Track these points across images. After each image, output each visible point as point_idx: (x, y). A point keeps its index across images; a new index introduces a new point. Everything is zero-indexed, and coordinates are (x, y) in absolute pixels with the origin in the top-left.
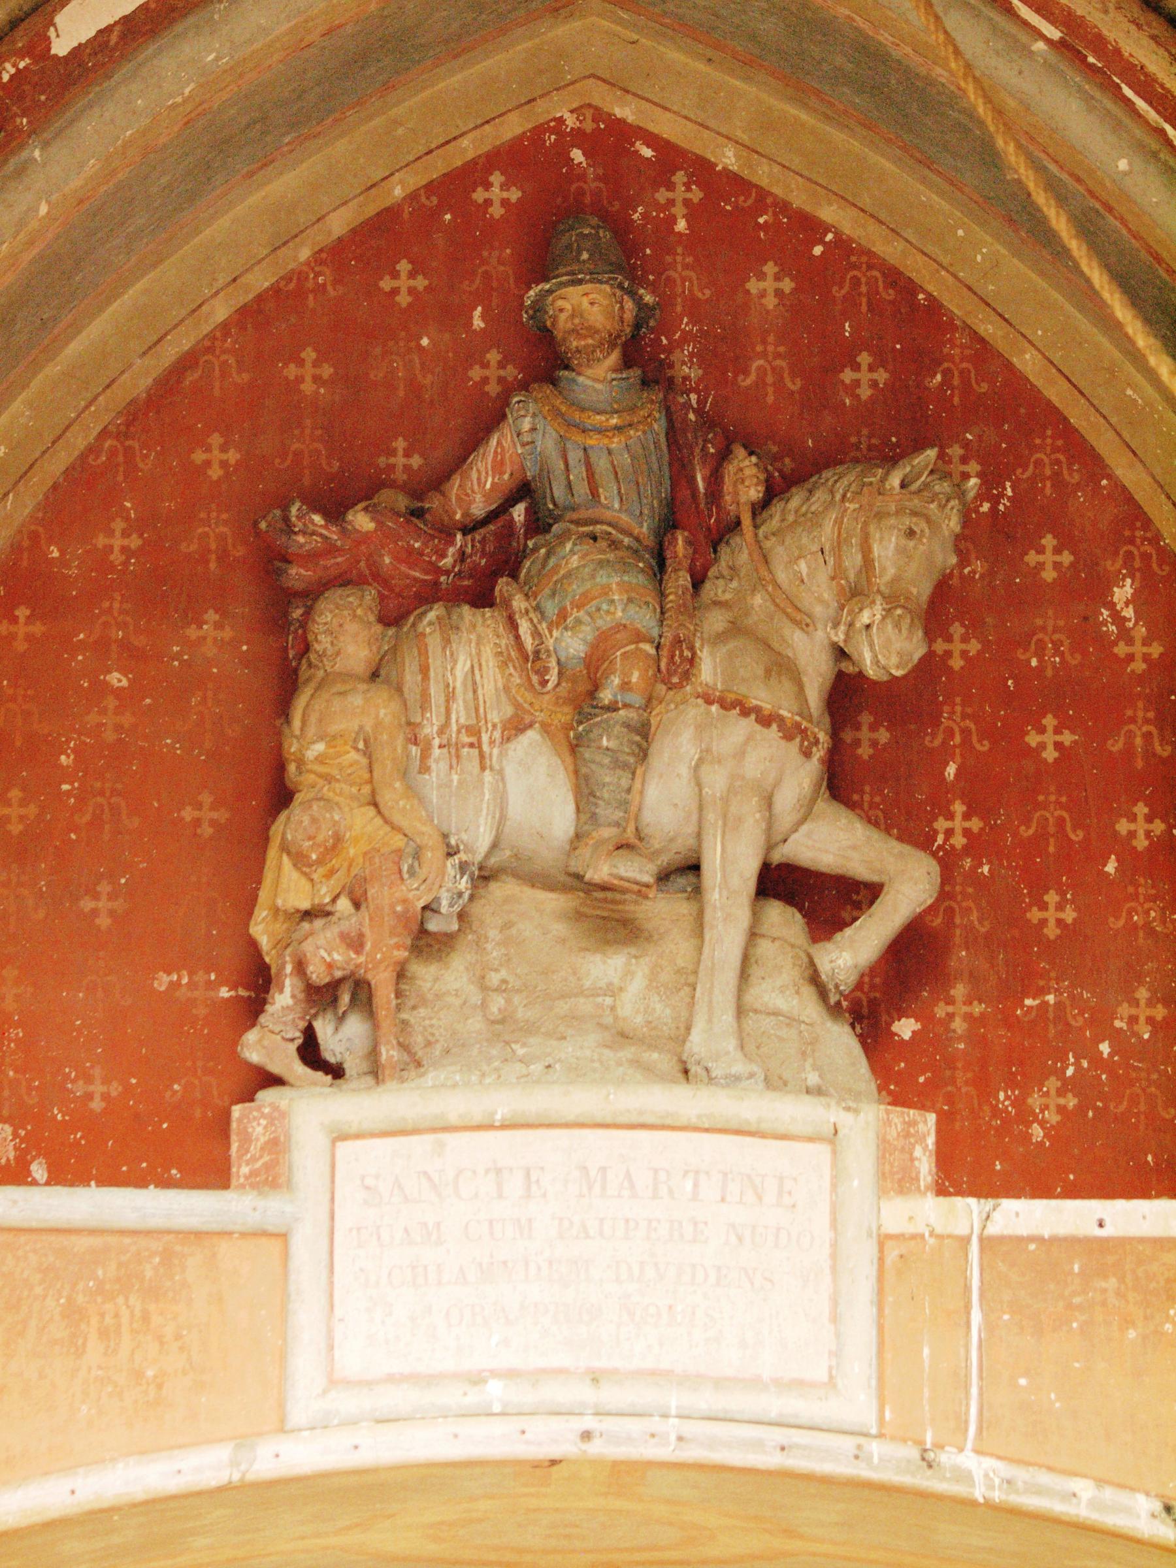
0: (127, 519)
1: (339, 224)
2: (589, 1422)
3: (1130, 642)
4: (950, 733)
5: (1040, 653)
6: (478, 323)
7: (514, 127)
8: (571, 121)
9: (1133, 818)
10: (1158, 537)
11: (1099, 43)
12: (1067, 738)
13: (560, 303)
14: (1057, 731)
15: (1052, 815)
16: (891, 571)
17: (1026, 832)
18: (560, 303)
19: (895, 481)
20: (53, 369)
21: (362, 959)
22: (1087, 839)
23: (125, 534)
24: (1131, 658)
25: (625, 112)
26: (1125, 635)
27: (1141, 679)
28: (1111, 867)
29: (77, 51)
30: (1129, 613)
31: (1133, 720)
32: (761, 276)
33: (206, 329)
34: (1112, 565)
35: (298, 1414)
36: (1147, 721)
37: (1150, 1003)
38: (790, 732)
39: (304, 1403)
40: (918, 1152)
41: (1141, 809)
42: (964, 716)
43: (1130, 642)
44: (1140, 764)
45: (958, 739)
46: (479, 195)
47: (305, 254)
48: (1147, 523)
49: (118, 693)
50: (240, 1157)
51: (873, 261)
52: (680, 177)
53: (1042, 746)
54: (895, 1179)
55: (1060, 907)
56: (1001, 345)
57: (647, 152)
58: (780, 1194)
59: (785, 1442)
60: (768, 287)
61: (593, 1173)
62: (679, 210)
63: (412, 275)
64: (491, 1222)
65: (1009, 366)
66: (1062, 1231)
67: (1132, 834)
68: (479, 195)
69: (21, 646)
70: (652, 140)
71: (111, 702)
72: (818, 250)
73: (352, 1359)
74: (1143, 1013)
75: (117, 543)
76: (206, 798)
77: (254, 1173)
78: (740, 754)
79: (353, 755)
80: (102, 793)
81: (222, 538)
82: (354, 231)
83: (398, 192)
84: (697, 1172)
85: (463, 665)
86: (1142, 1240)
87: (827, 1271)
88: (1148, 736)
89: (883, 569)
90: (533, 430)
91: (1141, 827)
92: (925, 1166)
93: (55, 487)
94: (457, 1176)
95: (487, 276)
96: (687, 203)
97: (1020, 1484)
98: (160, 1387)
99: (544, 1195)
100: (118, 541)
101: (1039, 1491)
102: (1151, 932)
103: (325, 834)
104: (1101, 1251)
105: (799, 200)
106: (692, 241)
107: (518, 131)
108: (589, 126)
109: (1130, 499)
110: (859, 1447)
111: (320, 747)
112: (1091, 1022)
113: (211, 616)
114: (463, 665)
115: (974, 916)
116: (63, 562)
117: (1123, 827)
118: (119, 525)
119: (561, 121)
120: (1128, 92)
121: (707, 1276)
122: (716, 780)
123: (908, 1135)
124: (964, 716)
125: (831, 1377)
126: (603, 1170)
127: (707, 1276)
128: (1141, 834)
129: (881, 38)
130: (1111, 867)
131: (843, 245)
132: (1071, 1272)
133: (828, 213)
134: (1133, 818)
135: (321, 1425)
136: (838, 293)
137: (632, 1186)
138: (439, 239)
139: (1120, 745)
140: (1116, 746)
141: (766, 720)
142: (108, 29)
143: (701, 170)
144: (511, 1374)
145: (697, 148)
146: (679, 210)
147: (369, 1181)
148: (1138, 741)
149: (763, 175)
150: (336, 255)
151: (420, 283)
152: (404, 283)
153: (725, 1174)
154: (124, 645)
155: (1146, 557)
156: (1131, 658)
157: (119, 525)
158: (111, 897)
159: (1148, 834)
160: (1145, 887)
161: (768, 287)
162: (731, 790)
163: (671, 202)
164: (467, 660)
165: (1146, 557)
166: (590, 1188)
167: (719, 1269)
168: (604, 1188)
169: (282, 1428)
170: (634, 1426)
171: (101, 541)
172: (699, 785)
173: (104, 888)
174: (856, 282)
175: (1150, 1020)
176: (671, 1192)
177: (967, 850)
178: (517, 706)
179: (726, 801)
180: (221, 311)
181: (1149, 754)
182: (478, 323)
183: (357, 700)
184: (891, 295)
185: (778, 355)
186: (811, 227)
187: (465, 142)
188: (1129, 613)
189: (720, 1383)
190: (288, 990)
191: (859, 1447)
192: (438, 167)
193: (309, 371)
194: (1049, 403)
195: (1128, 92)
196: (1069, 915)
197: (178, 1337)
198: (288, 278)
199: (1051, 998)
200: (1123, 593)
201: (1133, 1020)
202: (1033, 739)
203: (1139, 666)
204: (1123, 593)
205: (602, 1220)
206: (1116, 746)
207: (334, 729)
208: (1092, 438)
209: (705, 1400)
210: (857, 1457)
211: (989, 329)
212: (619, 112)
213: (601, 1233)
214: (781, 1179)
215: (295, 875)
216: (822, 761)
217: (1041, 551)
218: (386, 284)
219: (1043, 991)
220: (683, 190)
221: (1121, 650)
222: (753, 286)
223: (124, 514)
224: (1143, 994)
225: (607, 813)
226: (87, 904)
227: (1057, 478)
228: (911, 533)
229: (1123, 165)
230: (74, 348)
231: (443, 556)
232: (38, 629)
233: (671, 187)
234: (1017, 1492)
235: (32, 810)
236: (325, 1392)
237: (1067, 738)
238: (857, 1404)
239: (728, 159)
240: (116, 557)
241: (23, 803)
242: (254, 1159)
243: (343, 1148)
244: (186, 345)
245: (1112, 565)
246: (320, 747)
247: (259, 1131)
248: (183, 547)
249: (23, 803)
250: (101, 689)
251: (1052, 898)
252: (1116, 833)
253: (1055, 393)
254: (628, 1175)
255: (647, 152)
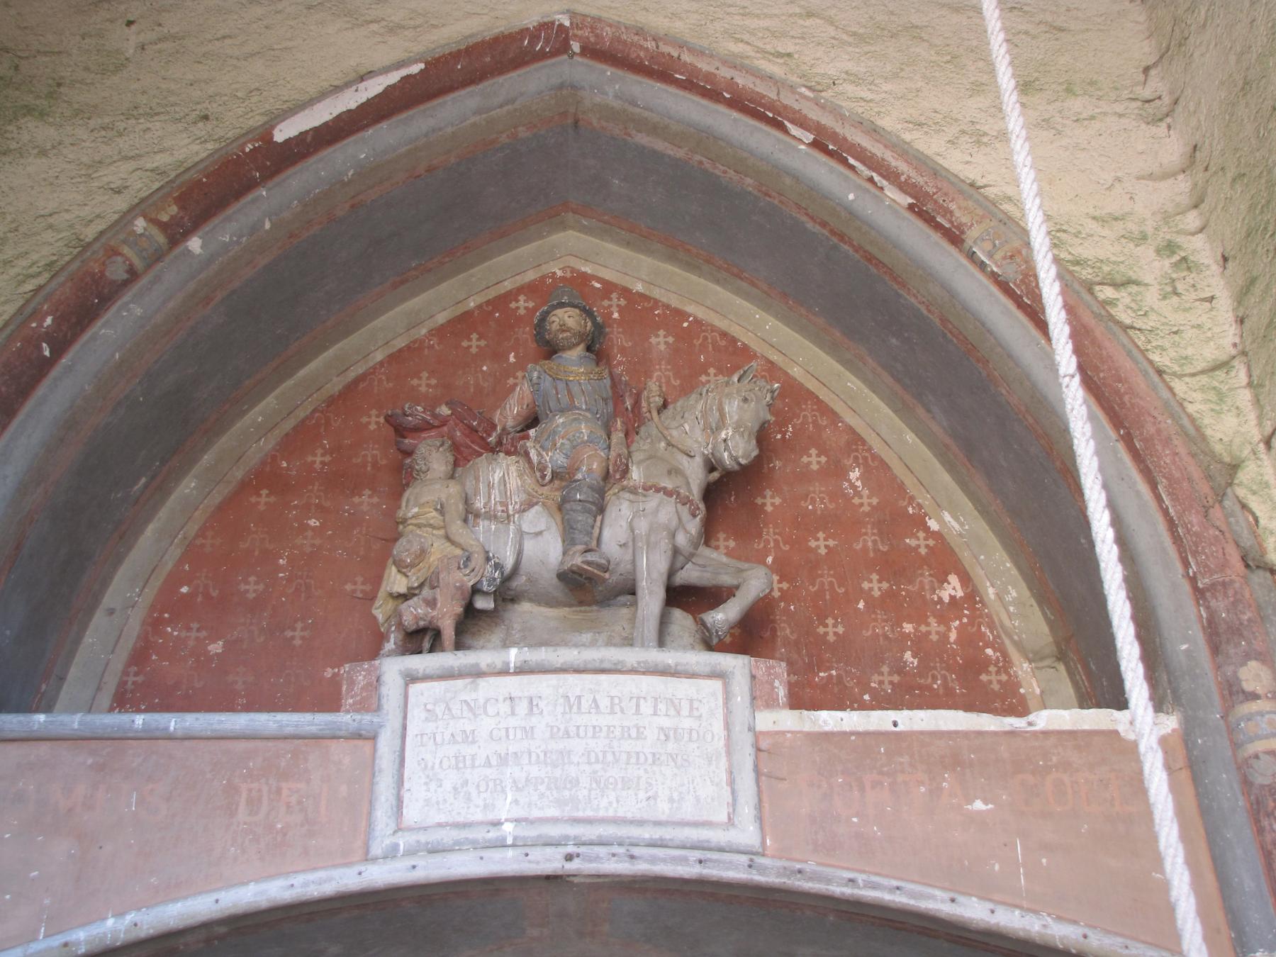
0: (324, 448)
1: (441, 318)
2: (571, 849)
3: (861, 497)
4: (767, 542)
5: (813, 502)
6: (512, 359)
7: (531, 276)
8: (559, 273)
9: (871, 581)
10: (870, 449)
11: (834, 137)
12: (831, 543)
13: (554, 318)
14: (825, 539)
15: (826, 580)
16: (736, 418)
17: (813, 589)
18: (554, 318)
19: (735, 379)
20: (290, 382)
21: (435, 613)
22: (846, 592)
23: (323, 455)
24: (862, 505)
25: (587, 269)
26: (858, 494)
27: (867, 514)
28: (861, 605)
29: (288, 141)
30: (859, 483)
31: (866, 534)
32: (657, 336)
33: (371, 364)
34: (848, 462)
35: (376, 849)
36: (873, 534)
37: (890, 674)
38: (685, 501)
39: (383, 834)
40: (777, 683)
41: (875, 577)
42: (775, 534)
43: (861, 497)
44: (872, 555)
45: (772, 544)
46: (513, 305)
47: (424, 331)
48: (864, 442)
49: (314, 529)
50: (348, 693)
51: (714, 329)
52: (614, 296)
53: (818, 547)
54: (760, 698)
55: (835, 626)
56: (781, 365)
57: (598, 285)
58: (691, 709)
59: (702, 857)
60: (660, 341)
61: (572, 700)
62: (615, 309)
63: (478, 340)
64: (507, 729)
65: (786, 373)
66: (871, 728)
67: (871, 589)
68: (513, 305)
69: (262, 508)
70: (599, 280)
71: (310, 533)
72: (685, 325)
73: (412, 814)
74: (886, 679)
75: (319, 459)
76: (359, 579)
77: (354, 704)
78: (657, 511)
79: (434, 514)
80: (301, 577)
81: (374, 456)
82: (449, 321)
83: (472, 304)
84: (638, 698)
85: (498, 475)
86: (922, 733)
87: (724, 754)
88: (875, 542)
89: (731, 417)
90: (539, 378)
91: (875, 585)
92: (782, 692)
93: (287, 435)
94: (485, 703)
95: (517, 339)
96: (618, 306)
97: (860, 881)
98: (285, 835)
99: (541, 713)
100: (318, 459)
101: (875, 886)
102: (886, 637)
103: (416, 547)
104: (895, 739)
105: (675, 302)
106: (620, 323)
107: (533, 278)
108: (568, 275)
109: (853, 432)
110: (751, 860)
111: (416, 510)
112: (858, 684)
113: (367, 492)
114: (498, 475)
115: (788, 631)
116: (288, 469)
117: (866, 585)
118: (319, 451)
119: (554, 273)
120: (851, 161)
121: (646, 759)
122: (642, 526)
123: (770, 674)
124: (775, 534)
125: (729, 818)
126: (579, 697)
127: (646, 759)
128: (876, 589)
129: (716, 172)
130: (861, 605)
131: (698, 322)
132: (879, 752)
133: (690, 309)
134: (871, 581)
135: (391, 854)
136: (697, 342)
137: (597, 707)
138: (492, 324)
139: (860, 546)
140: (858, 546)
141: (668, 493)
142: (307, 132)
143: (626, 292)
144: (504, 672)
145: (624, 284)
146: (615, 309)
147: (429, 707)
148: (870, 544)
149: (656, 293)
150: (440, 332)
151: (483, 343)
152: (474, 343)
153: (656, 699)
154: (319, 506)
155: (865, 459)
156: (862, 505)
157: (319, 451)
158: (303, 629)
159: (880, 589)
160: (880, 615)
161: (660, 341)
162: (651, 530)
163: (611, 306)
164: (501, 477)
165: (865, 459)
166: (571, 708)
167: (654, 754)
168: (579, 708)
169: (367, 858)
170: (602, 851)
171: (310, 459)
172: (633, 531)
173: (299, 625)
174: (706, 338)
175: (891, 683)
176: (622, 711)
177: (782, 598)
178: (529, 494)
179: (648, 536)
180: (379, 356)
181: (876, 550)
182: (512, 359)
183: (437, 486)
184: (723, 343)
185: (667, 370)
186: (682, 315)
187: (506, 283)
188: (859, 483)
189: (658, 823)
190: (392, 640)
191: (751, 860)
192: (492, 294)
193: (424, 382)
194: (808, 390)
195: (851, 161)
196: (840, 630)
197: (300, 803)
198: (415, 342)
199: (834, 672)
200: (854, 475)
201: (881, 683)
202: (813, 544)
203: (866, 508)
204: (854, 475)
205: (578, 727)
206: (858, 546)
207: (423, 500)
208: (831, 405)
209: (647, 833)
210: (750, 866)
211: (775, 357)
212: (583, 269)
213: (578, 735)
214: (691, 701)
215: (399, 576)
216: (701, 520)
217: (810, 456)
218: (465, 344)
219: (830, 668)
220: (616, 301)
221: (856, 501)
222: (653, 340)
223: (323, 447)
224: (885, 669)
225: (579, 537)
226: (289, 634)
227: (815, 423)
228: (745, 400)
229: (851, 197)
230: (302, 373)
231: (490, 435)
232: (272, 499)
233: (610, 299)
234: (859, 888)
235: (261, 587)
236: (395, 832)
237: (831, 543)
238: (747, 833)
239: (639, 287)
240: (317, 466)
241: (257, 583)
242: (356, 695)
243: (415, 689)
244: (360, 371)
245: (848, 462)
246: (416, 510)
247: (361, 679)
248: (354, 460)
249: (257, 583)
250: (304, 528)
251: (830, 621)
252: (862, 589)
253: (811, 385)
254: (595, 700)
255: (598, 285)
